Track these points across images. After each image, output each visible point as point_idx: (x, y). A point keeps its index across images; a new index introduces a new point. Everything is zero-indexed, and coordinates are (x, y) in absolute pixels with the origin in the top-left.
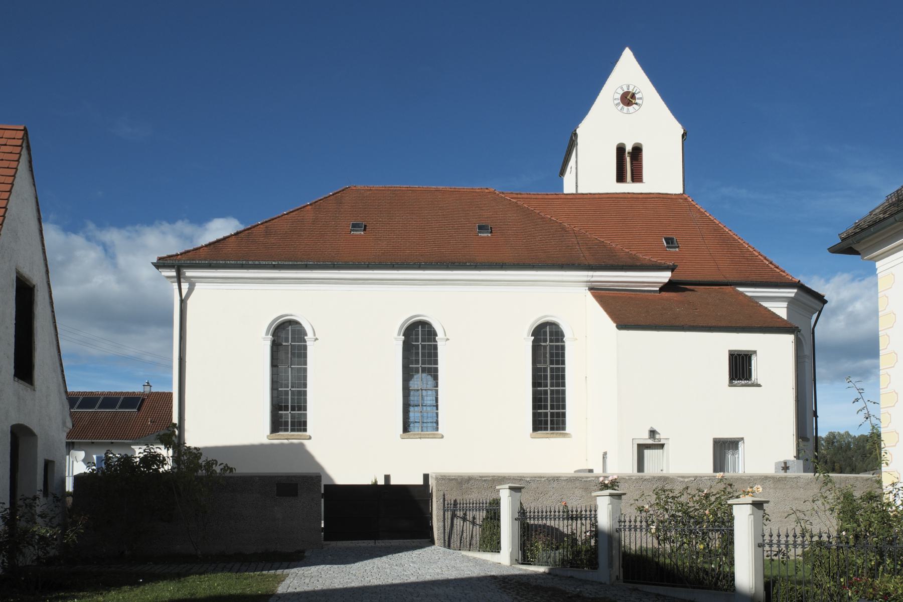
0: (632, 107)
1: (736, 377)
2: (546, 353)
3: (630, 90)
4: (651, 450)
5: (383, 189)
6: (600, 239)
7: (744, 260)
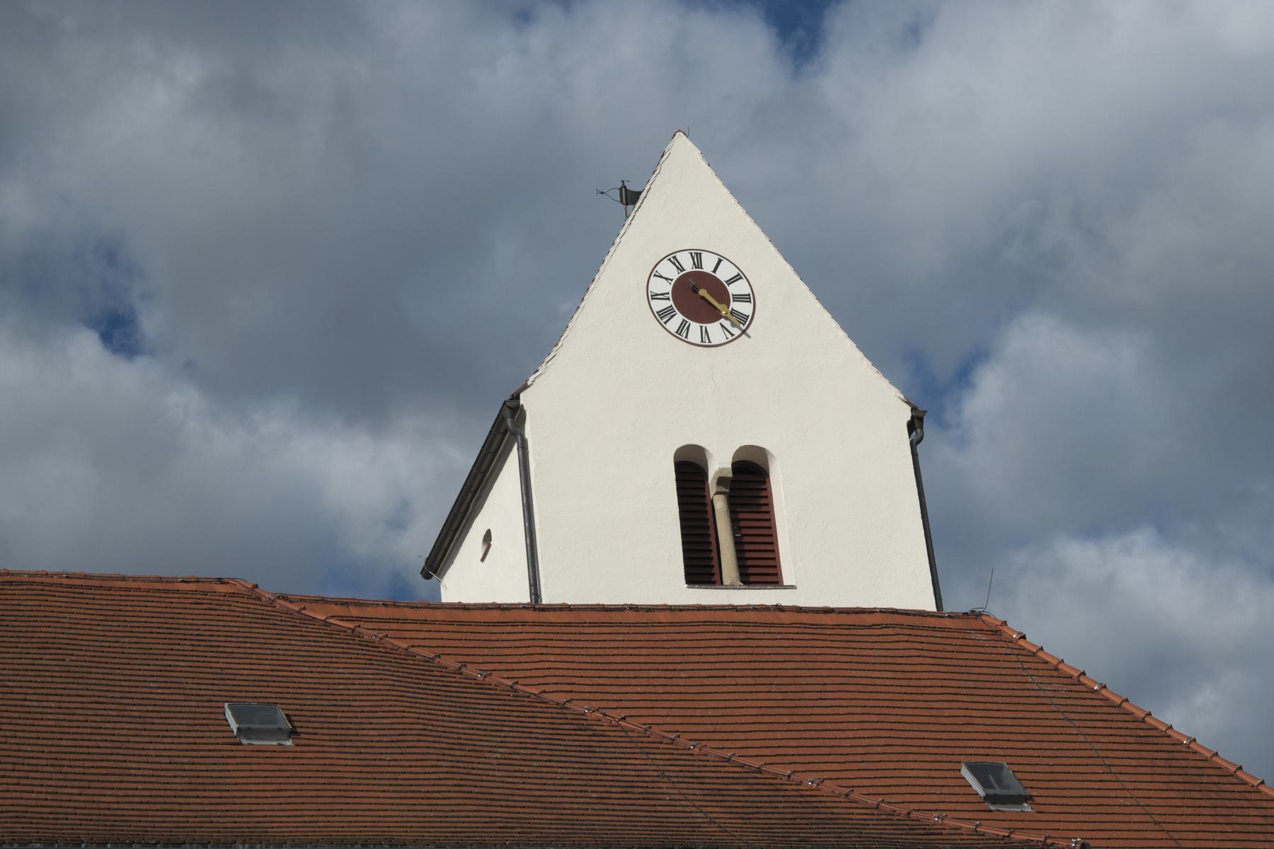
6: (742, 761)
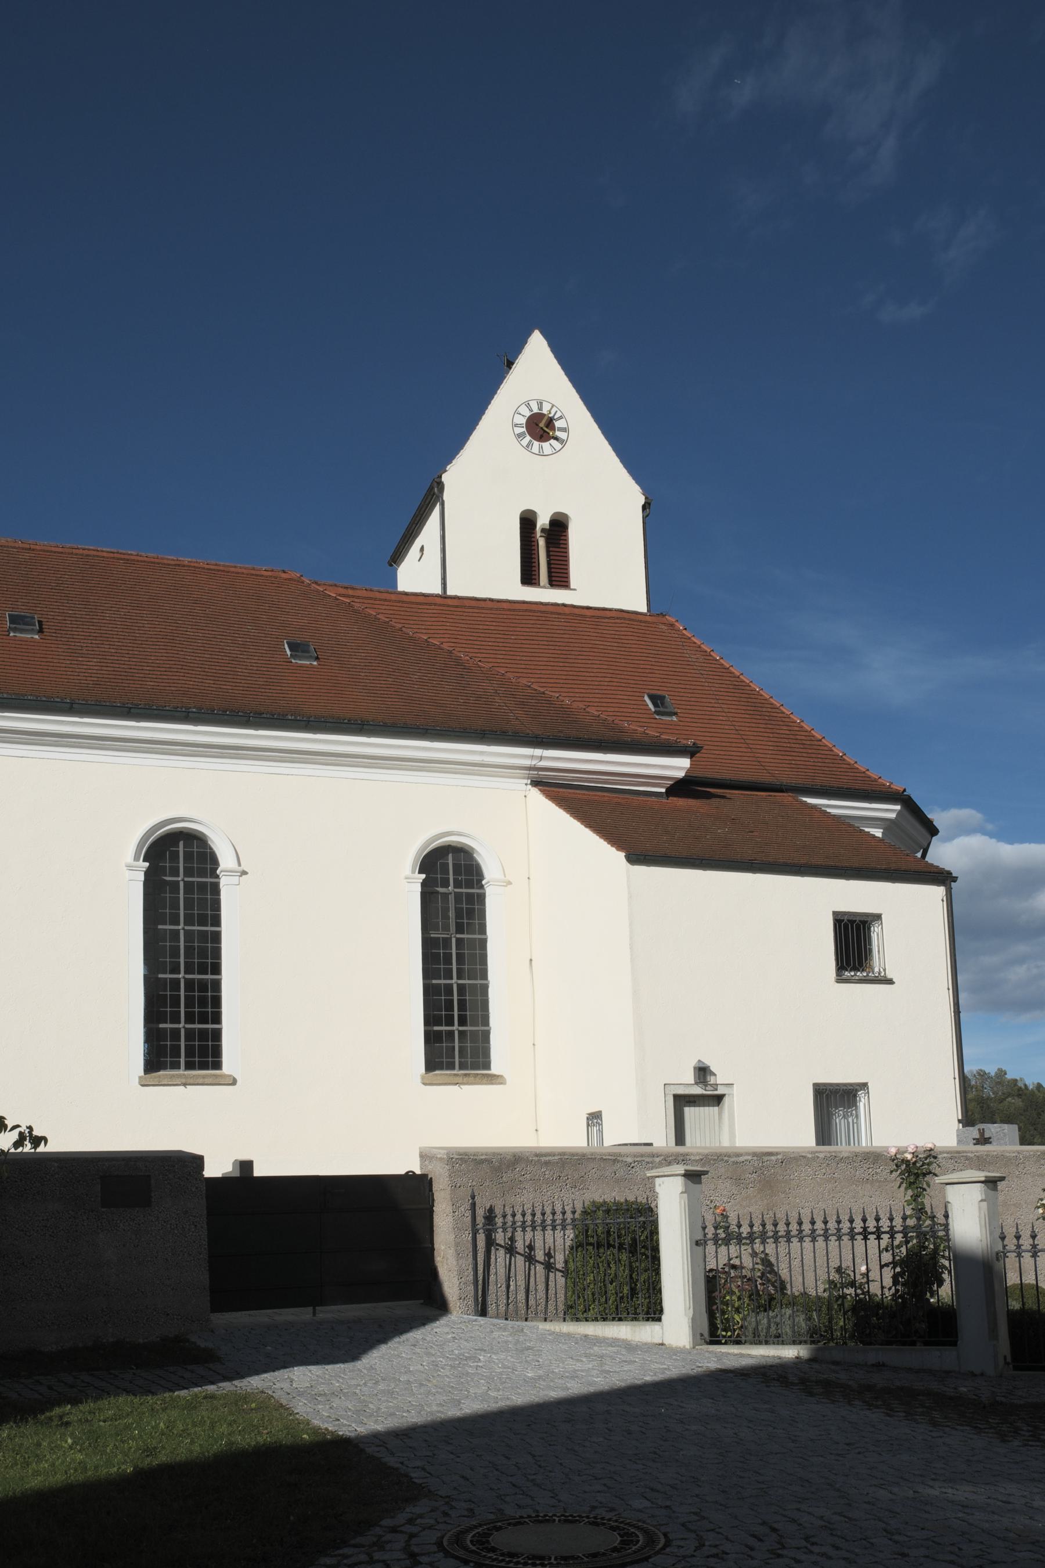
0: (548, 443)
1: (848, 964)
2: (448, 909)
3: (545, 411)
4: (697, 1109)
5: (60, 550)
7: (797, 746)
